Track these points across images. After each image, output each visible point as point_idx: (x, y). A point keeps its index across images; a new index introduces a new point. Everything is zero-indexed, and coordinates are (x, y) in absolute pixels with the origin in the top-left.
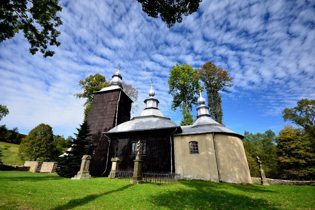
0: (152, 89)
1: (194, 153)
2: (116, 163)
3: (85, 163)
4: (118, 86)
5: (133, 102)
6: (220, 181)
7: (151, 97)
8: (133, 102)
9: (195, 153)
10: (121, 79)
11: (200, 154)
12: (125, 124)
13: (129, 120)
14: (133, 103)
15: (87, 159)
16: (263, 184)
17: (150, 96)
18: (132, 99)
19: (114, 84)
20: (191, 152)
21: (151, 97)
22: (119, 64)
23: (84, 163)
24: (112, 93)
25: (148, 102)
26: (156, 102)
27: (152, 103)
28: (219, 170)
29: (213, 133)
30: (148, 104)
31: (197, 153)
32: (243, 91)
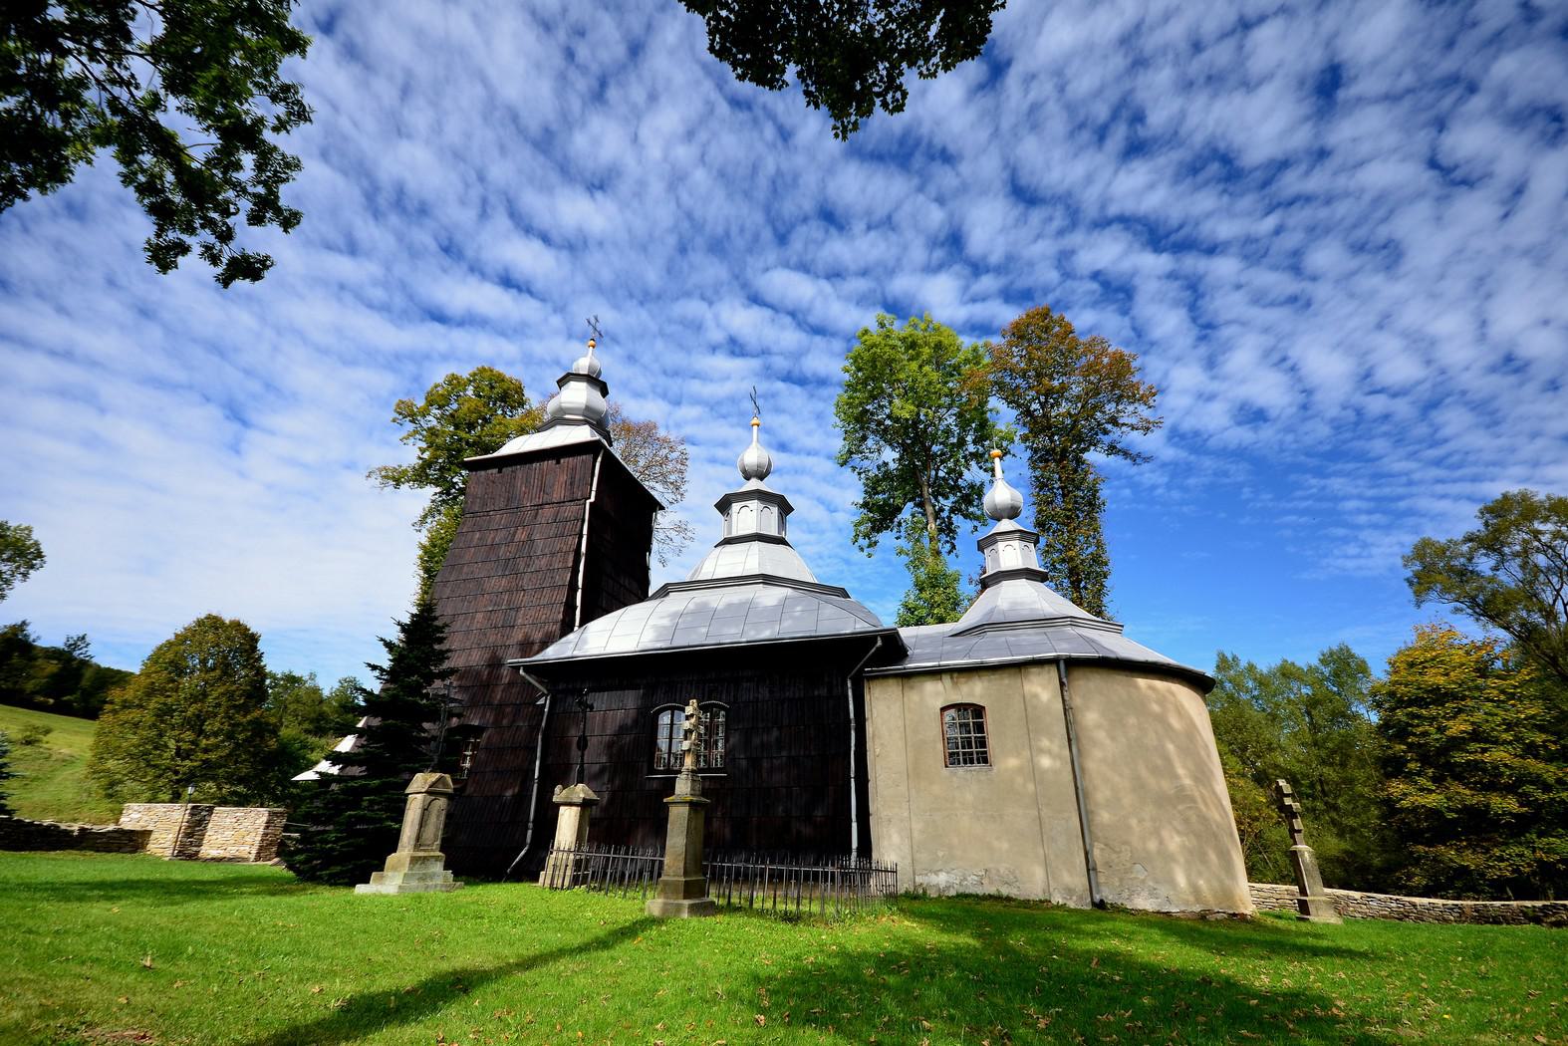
0: (754, 443)
5: (662, 508)
6: (1094, 904)
8: (662, 508)
10: (604, 392)
11: (945, 772)
15: (432, 792)
18: (658, 491)
19: (567, 416)
21: (754, 484)
23: (419, 811)
25: (735, 507)
26: (775, 510)
27: (755, 512)
28: (1088, 847)
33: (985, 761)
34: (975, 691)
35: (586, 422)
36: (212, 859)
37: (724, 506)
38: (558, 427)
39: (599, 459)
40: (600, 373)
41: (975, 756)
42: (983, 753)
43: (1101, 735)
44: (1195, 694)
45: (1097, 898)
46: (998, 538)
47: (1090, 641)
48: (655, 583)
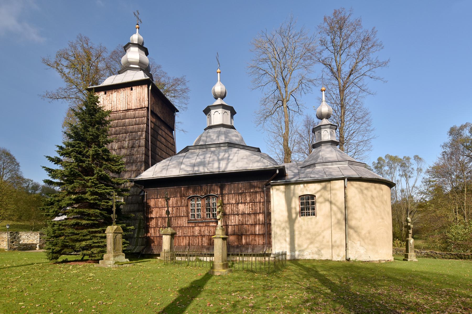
0: (219, 82)
1: (307, 215)
2: (168, 237)
3: (115, 239)
4: (142, 71)
5: (178, 111)
6: (346, 259)
7: (219, 102)
8: (178, 111)
9: (309, 215)
10: (147, 54)
11: (317, 217)
12: (156, 167)
13: (174, 153)
14: (177, 113)
15: (115, 233)
16: (408, 253)
17: (216, 98)
18: (176, 103)
19: (131, 66)
20: (236, 113)
21: (219, 102)
22: (136, 14)
23: (112, 240)
24: (132, 89)
25: (213, 111)
26: (229, 112)
27: (221, 114)
28: (347, 242)
29: (346, 179)
30: (212, 116)
31: (312, 215)
32: (85, 215)
33: (314, 215)
34: (312, 189)
35: (141, 69)
36: (114, 246)
37: (207, 111)
38: (128, 71)
39: (150, 87)
40: (143, 43)
41: (310, 213)
42: (304, 215)
43: (109, 246)
44: (388, 187)
45: (348, 258)
46: (322, 127)
47: (374, 175)
48: (179, 148)
